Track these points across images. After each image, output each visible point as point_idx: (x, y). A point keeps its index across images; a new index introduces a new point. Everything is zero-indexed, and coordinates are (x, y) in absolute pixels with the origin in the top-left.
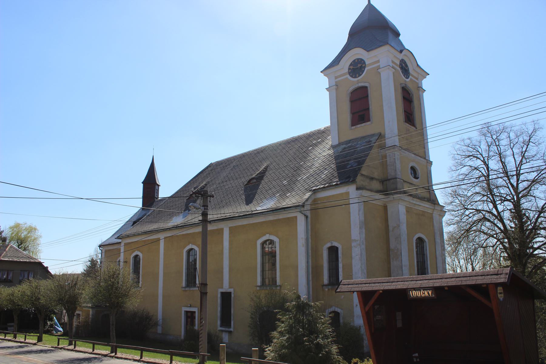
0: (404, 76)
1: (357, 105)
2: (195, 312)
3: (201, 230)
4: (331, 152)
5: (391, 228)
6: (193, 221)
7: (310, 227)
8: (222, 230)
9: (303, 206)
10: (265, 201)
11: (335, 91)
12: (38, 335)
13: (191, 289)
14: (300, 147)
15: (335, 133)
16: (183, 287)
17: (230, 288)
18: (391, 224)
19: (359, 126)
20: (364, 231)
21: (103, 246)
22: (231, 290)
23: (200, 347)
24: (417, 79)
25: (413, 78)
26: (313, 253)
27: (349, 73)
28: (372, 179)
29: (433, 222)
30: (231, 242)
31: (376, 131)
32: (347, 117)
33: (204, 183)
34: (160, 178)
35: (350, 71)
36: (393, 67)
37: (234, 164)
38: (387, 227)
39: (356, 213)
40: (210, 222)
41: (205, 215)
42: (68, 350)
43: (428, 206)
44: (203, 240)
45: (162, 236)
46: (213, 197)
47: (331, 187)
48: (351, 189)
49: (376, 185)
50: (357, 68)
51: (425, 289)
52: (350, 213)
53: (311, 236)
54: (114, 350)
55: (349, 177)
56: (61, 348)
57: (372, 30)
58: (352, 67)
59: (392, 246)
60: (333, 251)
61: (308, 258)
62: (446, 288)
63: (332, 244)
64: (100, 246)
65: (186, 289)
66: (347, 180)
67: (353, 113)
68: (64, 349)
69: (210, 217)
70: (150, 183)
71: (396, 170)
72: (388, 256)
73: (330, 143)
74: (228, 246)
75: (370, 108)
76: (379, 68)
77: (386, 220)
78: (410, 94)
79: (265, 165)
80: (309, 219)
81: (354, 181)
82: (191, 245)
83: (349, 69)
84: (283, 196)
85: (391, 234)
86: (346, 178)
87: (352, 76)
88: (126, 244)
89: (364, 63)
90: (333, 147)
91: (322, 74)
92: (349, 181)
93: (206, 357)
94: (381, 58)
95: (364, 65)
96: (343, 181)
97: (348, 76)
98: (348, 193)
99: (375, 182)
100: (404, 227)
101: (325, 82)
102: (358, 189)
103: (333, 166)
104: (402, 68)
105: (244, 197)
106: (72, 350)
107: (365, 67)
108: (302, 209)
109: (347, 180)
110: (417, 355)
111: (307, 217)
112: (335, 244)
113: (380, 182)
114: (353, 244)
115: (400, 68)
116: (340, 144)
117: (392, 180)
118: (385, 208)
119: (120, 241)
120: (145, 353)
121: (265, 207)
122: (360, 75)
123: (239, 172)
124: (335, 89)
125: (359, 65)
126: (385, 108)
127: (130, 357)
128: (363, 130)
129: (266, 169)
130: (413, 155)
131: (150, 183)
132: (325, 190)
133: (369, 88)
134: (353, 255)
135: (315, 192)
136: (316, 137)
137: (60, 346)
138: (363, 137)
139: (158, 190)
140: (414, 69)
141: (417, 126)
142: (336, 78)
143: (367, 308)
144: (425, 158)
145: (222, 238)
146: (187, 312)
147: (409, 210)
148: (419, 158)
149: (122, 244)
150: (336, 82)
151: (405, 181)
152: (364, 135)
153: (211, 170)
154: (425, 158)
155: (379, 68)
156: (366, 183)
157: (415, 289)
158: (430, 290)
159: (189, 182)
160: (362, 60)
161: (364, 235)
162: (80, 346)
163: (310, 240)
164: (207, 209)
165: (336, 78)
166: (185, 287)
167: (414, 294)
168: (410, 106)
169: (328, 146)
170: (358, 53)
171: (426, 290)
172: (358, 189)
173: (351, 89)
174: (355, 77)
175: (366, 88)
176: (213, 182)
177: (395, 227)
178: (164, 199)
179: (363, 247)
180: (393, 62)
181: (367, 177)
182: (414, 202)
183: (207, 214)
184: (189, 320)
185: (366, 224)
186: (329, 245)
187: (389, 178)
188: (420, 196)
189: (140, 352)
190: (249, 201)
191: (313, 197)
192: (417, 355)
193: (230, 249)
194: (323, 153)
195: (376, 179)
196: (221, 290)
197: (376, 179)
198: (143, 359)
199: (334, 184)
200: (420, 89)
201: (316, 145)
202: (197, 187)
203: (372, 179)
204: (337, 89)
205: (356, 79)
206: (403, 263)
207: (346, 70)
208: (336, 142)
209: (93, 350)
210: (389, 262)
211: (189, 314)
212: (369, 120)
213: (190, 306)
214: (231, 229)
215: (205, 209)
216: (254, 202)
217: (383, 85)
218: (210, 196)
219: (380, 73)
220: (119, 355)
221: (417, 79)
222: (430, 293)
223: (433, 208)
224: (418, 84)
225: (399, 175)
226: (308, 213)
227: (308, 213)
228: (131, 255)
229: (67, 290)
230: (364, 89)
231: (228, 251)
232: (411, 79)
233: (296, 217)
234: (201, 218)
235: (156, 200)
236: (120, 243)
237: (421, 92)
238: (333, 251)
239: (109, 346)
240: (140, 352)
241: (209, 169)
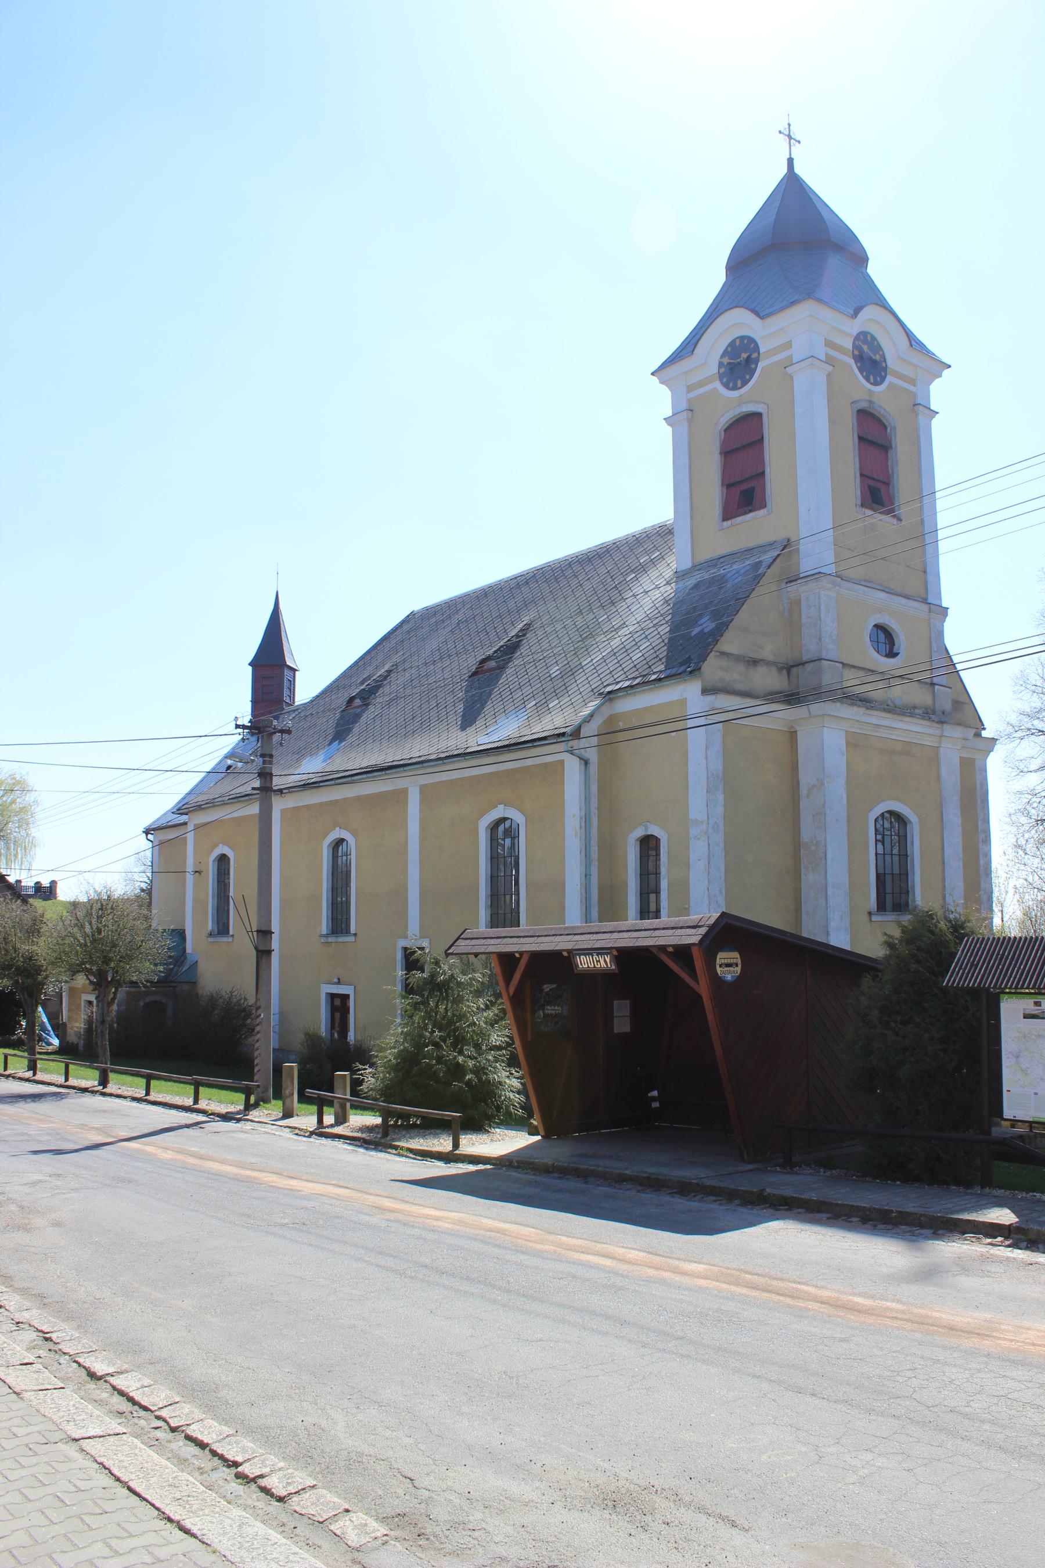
0: (868, 379)
1: (737, 466)
2: (347, 996)
3: (257, 811)
4: (669, 590)
5: (803, 790)
6: (238, 791)
7: (594, 788)
8: (404, 792)
9: (576, 734)
10: (502, 721)
11: (685, 425)
12: (81, 1048)
13: (341, 939)
14: (595, 575)
15: (682, 541)
16: (324, 936)
17: (421, 937)
18: (806, 778)
19: (739, 519)
20: (720, 798)
21: (154, 830)
22: (425, 943)
23: (256, 1070)
24: (912, 382)
25: (896, 381)
26: (603, 851)
27: (721, 377)
28: (754, 662)
29: (938, 769)
30: (423, 822)
31: (778, 534)
32: (714, 495)
33: (387, 667)
34: (298, 650)
35: (722, 370)
36: (829, 360)
37: (460, 616)
38: (795, 785)
39: (701, 751)
40: (281, 791)
41: (265, 775)
42: (21, 1079)
43: (927, 731)
44: (261, 833)
45: (412, 785)
46: (289, 732)
47: (645, 684)
48: (688, 694)
49: (767, 679)
50: (740, 362)
51: (601, 951)
52: (686, 752)
53: (599, 809)
54: (104, 1081)
55: (688, 661)
56: (8, 1076)
57: (795, 247)
58: (726, 361)
59: (806, 834)
60: (649, 845)
61: (587, 865)
62: (671, 949)
63: (646, 829)
64: (147, 832)
65: (330, 940)
66: (682, 668)
67: (728, 485)
68: (14, 1077)
69: (277, 782)
70: (271, 665)
71: (820, 640)
72: (797, 858)
73: (674, 565)
74: (417, 834)
75: (767, 471)
76: (789, 363)
77: (794, 768)
78: (885, 428)
79: (526, 620)
80: (593, 769)
81: (695, 672)
82: (337, 829)
83: (721, 365)
84: (543, 707)
85: (804, 803)
86: (681, 664)
87: (726, 386)
88: (197, 828)
89: (757, 349)
90: (680, 576)
91: (655, 379)
92: (685, 671)
93: (348, 1105)
94: (801, 334)
95: (754, 356)
96: (674, 671)
97: (717, 385)
98: (683, 702)
99: (762, 670)
100: (837, 790)
101: (661, 400)
102: (705, 691)
103: (665, 629)
104: (860, 358)
105: (461, 707)
106: (27, 1080)
107: (757, 361)
108: (575, 743)
109: (682, 668)
110: (655, 1093)
111: (586, 763)
112: (654, 830)
113: (780, 670)
114: (693, 832)
115: (854, 357)
116: (696, 567)
117: (811, 665)
118: (792, 736)
119: (184, 818)
120: (154, 1083)
121: (495, 738)
122: (745, 383)
123: (467, 639)
124: (686, 417)
125: (744, 355)
126: (801, 472)
127: (126, 1094)
128: (754, 529)
129: (524, 631)
130: (882, 595)
131: (271, 665)
132: (634, 694)
133: (765, 418)
134: (693, 857)
135: (609, 697)
136: (650, 543)
137: (7, 1073)
138: (749, 550)
139: (292, 683)
140: (900, 358)
141: (902, 511)
142: (690, 389)
143: (512, 989)
144: (925, 601)
145: (406, 812)
146: (332, 996)
147: (854, 743)
148: (904, 601)
149: (190, 827)
150: (689, 401)
151: (844, 665)
152: (751, 545)
153: (408, 632)
154: (925, 601)
155: (789, 363)
156: (735, 675)
157: (588, 952)
158: (607, 954)
159: (356, 663)
160: (751, 340)
161: (720, 810)
162: (45, 1070)
163: (595, 821)
164: (271, 763)
165: (690, 389)
166: (327, 936)
167: (584, 963)
168: (883, 462)
169: (668, 574)
170: (740, 322)
171: (601, 954)
172: (705, 691)
173: (726, 418)
174: (735, 388)
175: (757, 416)
176: (407, 665)
177: (814, 786)
178: (305, 706)
179: (719, 838)
180: (828, 344)
181: (738, 659)
182: (874, 721)
183: (271, 775)
184: (337, 1015)
185: (729, 782)
186: (640, 832)
187: (805, 659)
188: (898, 702)
189: (144, 1081)
190: (468, 720)
191: (606, 711)
192: (655, 1093)
193: (422, 840)
194: (654, 592)
195: (768, 663)
196: (402, 943)
197: (768, 663)
198: (202, 1104)
199: (654, 677)
200: (920, 410)
201: (643, 569)
202: (369, 678)
203: (754, 662)
204: (690, 421)
205: (735, 394)
206: (829, 877)
207: (713, 368)
208: (687, 564)
209: (67, 1080)
210: (797, 875)
211: (338, 1002)
212: (763, 505)
213: (339, 982)
214: (423, 789)
215: (264, 762)
216: (480, 723)
217: (798, 410)
218: (282, 731)
219: (791, 378)
220: (111, 1088)
221: (912, 382)
222: (608, 960)
223: (938, 732)
224: (914, 395)
225: (830, 650)
226: (592, 755)
227: (592, 755)
228: (209, 854)
229: (102, 935)
230: (753, 419)
231: (417, 846)
232: (891, 384)
233: (562, 762)
234: (257, 784)
235: (287, 709)
236: (185, 824)
237: (921, 419)
238: (649, 845)
239: (97, 1068)
240: (144, 1081)
241: (406, 627)
